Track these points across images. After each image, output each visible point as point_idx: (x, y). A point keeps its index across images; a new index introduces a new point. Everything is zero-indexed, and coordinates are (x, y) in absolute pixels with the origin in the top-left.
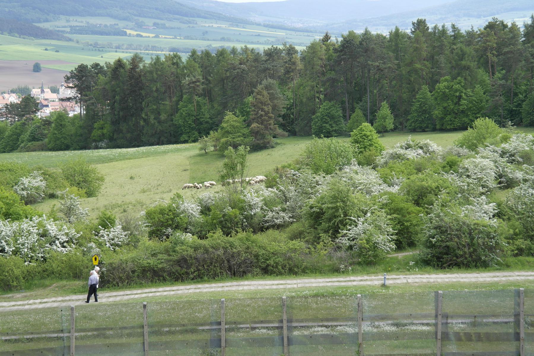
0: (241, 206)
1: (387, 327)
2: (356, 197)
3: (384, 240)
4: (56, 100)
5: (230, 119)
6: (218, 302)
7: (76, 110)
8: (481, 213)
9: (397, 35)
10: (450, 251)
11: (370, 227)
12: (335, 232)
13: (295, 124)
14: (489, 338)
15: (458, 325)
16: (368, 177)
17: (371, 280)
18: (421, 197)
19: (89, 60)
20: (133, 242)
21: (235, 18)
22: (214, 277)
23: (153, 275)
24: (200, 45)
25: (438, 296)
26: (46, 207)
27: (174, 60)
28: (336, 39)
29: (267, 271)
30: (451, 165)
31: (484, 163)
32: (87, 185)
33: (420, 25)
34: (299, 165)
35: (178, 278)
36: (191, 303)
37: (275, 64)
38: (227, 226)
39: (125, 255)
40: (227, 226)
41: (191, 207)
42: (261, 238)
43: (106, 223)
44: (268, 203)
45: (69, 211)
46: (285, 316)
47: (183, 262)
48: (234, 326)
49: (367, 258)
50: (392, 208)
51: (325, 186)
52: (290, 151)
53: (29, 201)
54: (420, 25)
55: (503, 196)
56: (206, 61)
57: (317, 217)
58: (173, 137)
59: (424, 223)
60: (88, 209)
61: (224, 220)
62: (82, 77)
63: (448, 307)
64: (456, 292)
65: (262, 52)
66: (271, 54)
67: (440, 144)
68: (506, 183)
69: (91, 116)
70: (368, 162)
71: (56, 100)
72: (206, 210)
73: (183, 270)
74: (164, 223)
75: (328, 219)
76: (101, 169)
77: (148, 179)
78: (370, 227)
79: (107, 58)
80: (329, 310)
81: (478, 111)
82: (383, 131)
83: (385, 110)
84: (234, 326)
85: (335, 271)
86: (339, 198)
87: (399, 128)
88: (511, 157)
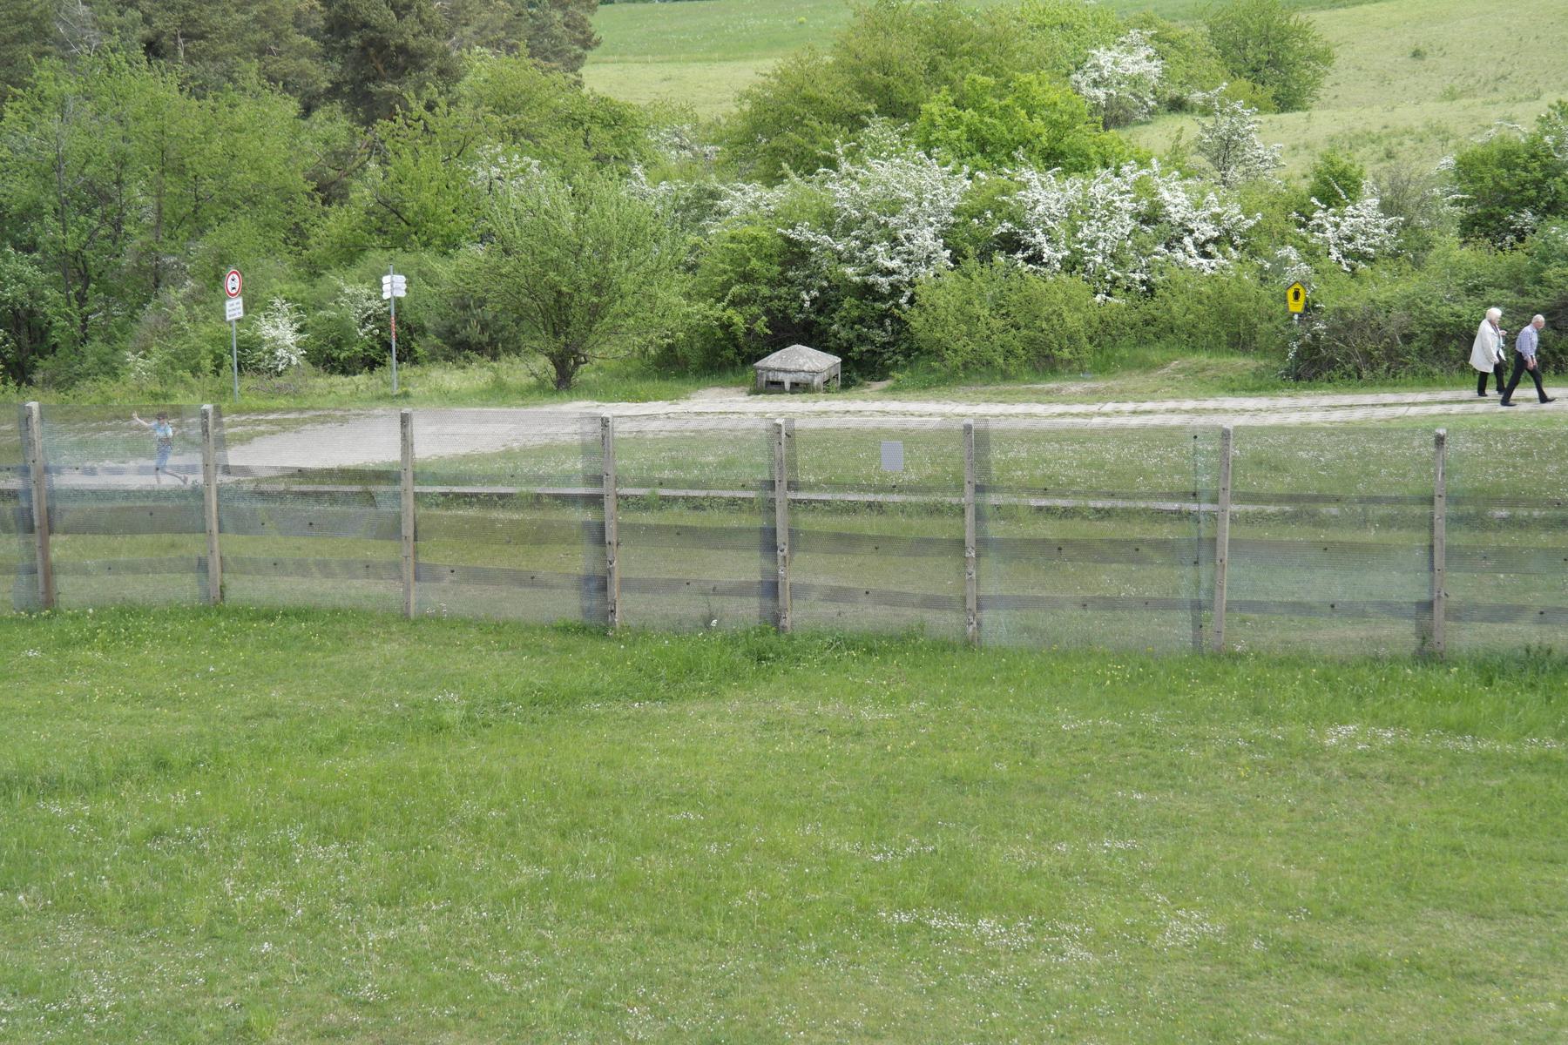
20: (1411, 249)
26: (1158, 135)
45: (1225, 151)
60: (1283, 145)
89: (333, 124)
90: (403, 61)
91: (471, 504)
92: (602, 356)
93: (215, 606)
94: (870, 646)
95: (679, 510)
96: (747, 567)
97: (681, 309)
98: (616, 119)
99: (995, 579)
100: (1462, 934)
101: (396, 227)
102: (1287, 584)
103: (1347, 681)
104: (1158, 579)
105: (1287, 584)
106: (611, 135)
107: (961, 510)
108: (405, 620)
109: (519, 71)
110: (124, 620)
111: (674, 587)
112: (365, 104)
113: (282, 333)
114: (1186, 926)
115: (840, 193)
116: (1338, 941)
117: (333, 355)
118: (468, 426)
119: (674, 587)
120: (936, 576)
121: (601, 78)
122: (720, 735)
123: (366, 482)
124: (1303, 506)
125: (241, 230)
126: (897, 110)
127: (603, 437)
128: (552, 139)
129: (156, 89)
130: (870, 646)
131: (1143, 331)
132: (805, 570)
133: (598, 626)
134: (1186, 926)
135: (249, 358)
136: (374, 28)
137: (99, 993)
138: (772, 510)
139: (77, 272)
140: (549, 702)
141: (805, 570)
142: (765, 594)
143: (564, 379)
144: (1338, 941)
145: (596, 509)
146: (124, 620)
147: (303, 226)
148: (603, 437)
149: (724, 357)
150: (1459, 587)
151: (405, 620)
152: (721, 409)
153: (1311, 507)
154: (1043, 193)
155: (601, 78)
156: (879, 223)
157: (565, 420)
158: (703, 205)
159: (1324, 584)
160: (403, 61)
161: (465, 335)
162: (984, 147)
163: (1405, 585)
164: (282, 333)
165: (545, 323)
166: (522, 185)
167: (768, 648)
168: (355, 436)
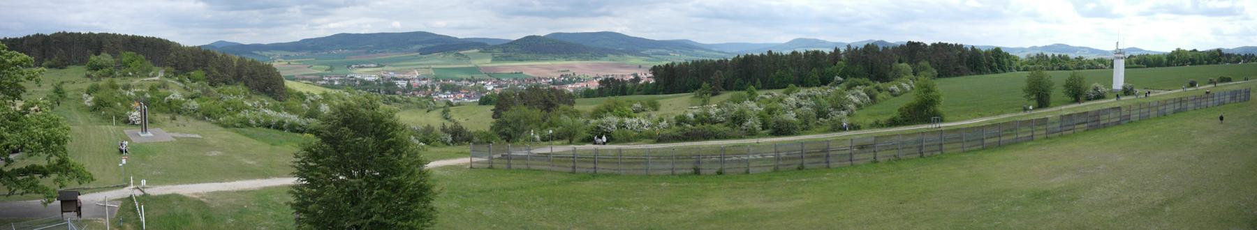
0: (708, 115)
1: (759, 157)
2: (748, 112)
3: (758, 127)
4: (646, 77)
5: (705, 84)
6: (698, 148)
7: (652, 81)
8: (791, 116)
9: (762, 55)
10: (779, 130)
11: (753, 123)
12: (741, 124)
13: (727, 86)
14: (794, 158)
15: (783, 155)
16: (752, 105)
17: (753, 141)
18: (770, 112)
19: (657, 64)
20: (670, 127)
21: (768, 19)
22: (698, 140)
23: (676, 139)
24: (695, 58)
25: (776, 145)
26: (642, 114)
27: (686, 64)
28: (742, 56)
29: (717, 138)
30: (781, 101)
31: (792, 99)
32: (655, 107)
33: (770, 52)
34: (728, 101)
35: (685, 140)
36: (690, 148)
37: (721, 65)
38: (703, 122)
39: (667, 132)
40: (703, 122)
41: (691, 115)
42: (715, 126)
43: (661, 120)
44: (717, 114)
45: (649, 116)
46: (723, 152)
47: (687, 134)
48: (705, 157)
49: (752, 133)
50: (760, 115)
51: (737, 107)
52: (726, 96)
53: (636, 112)
54: (770, 52)
55: (799, 110)
56: (697, 64)
57: (734, 119)
58: (685, 90)
59: (772, 120)
60: (655, 115)
61: (700, 120)
62: (655, 70)
63: (779, 149)
64: (781, 144)
65: (487, 129)
66: (720, 62)
67: (777, 93)
68: (799, 106)
69: (657, 83)
70: (752, 100)
71: (646, 77)
72: (695, 116)
73: (687, 137)
74: (681, 120)
75: (738, 120)
76: (660, 101)
77: (678, 105)
78: (753, 123)
79: (664, 63)
80: (738, 150)
81: (790, 81)
82: (758, 89)
83: (759, 81)
84: (705, 157)
85: (741, 138)
86: (741, 112)
87: (764, 88)
88: (801, 97)
89: (545, 112)
90: (553, 105)
91: (560, 158)
92: (575, 140)
93: (528, 169)
94: (607, 175)
95: (583, 158)
96: (592, 165)
97: (585, 134)
98: (577, 112)
99: (622, 167)
100: (677, 207)
101: (551, 125)
102: (657, 166)
103: (664, 178)
104: (642, 166)
105: (657, 166)
106: (577, 114)
107: (618, 158)
108: (550, 171)
109: (566, 106)
110: (518, 170)
111: (583, 168)
112: (548, 111)
113: (538, 137)
114: (645, 208)
115: (604, 121)
116: (663, 209)
117: (543, 139)
118: (559, 148)
119: (583, 168)
120: (615, 167)
121: (576, 107)
122: (589, 186)
123: (547, 154)
124: (659, 157)
125: (533, 125)
126: (611, 111)
127: (575, 150)
128: (77, 86)
129: (524, 109)
130: (607, 175)
131: (641, 137)
132: (600, 166)
133: (574, 172)
134: (645, 208)
135: (534, 140)
136: (579, 80)
137: (514, 214)
138: (595, 159)
139: (515, 130)
140: (568, 181)
141: (600, 166)
142: (595, 168)
143: (570, 143)
144: (663, 209)
145: (574, 158)
146: (518, 170)
147: (539, 125)
148: (575, 150)
149: (590, 140)
150: (676, 166)
151: (550, 171)
152: (590, 146)
153: (659, 157)
154: (627, 120)
155: (576, 107)
156: (608, 124)
157: (571, 147)
158: (587, 122)
159: (661, 166)
160: (553, 105)
161: (558, 137)
162: (621, 115)
163: (670, 166)
164: (538, 137)
165: (568, 136)
166: (566, 120)
167: (595, 175)
168: (546, 150)
